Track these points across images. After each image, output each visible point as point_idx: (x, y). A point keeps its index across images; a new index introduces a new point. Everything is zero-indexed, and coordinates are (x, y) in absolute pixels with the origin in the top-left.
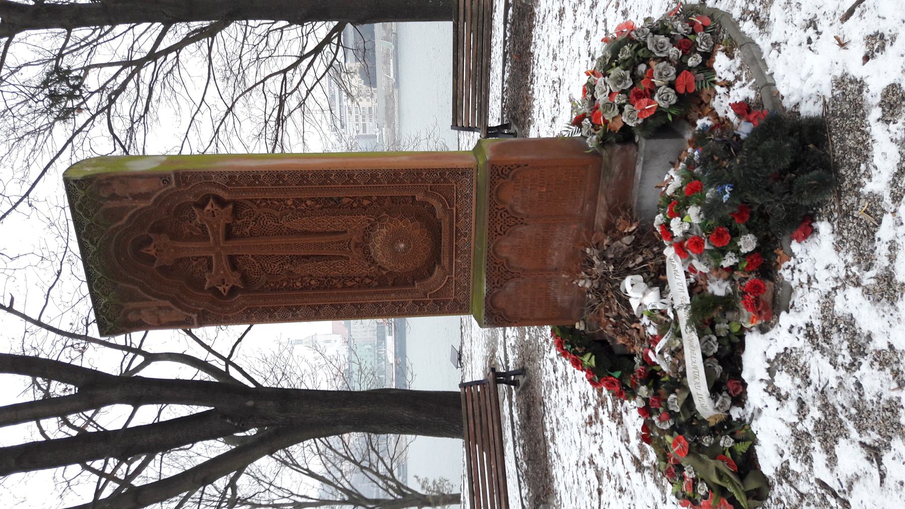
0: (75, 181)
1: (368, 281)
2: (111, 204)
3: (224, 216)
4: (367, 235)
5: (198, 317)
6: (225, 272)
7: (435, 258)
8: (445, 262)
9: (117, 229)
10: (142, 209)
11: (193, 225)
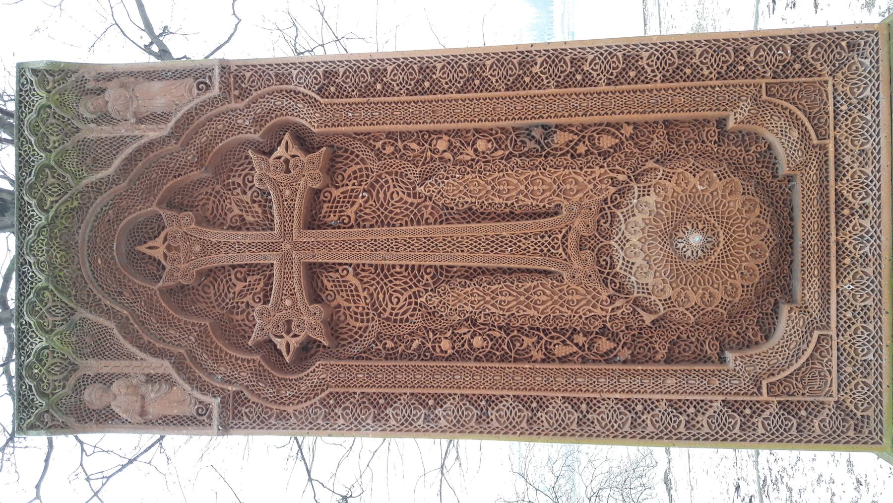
0: (35, 72)
1: (605, 345)
2: (92, 132)
3: (309, 171)
4: (607, 214)
5: (224, 405)
6: (295, 302)
7: (777, 285)
8: (806, 290)
9: (97, 188)
10: (150, 145)
11: (247, 198)
